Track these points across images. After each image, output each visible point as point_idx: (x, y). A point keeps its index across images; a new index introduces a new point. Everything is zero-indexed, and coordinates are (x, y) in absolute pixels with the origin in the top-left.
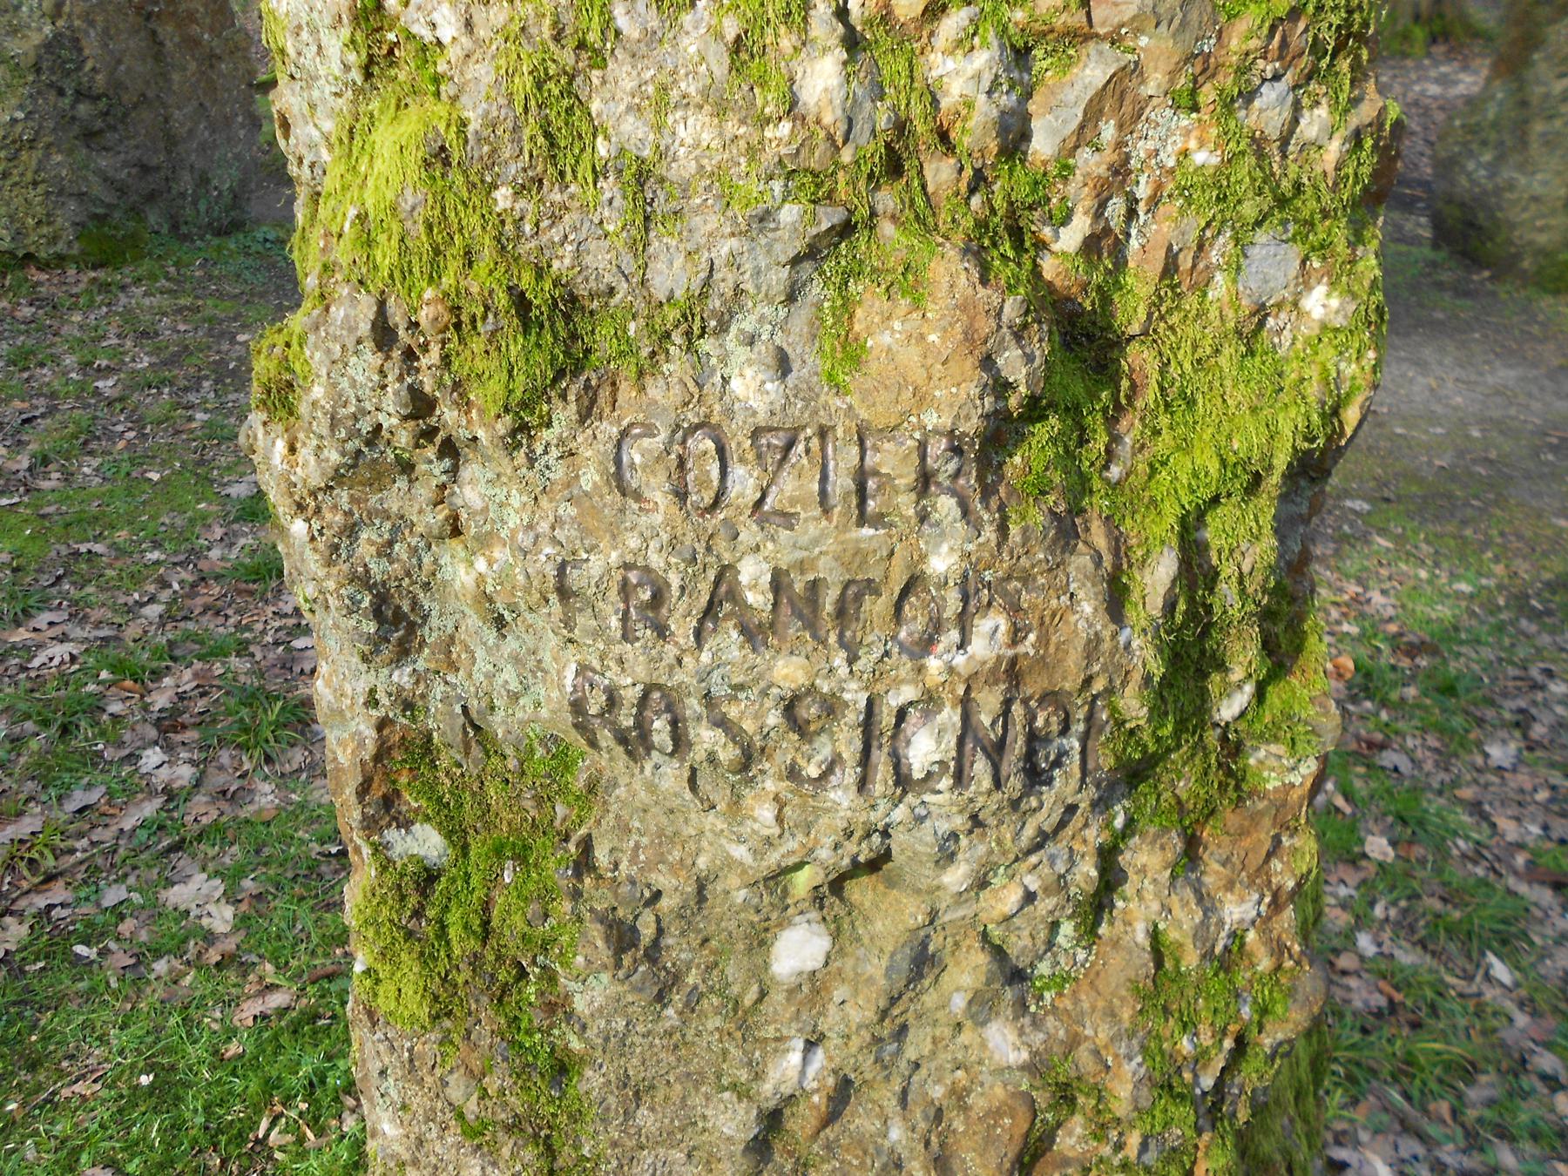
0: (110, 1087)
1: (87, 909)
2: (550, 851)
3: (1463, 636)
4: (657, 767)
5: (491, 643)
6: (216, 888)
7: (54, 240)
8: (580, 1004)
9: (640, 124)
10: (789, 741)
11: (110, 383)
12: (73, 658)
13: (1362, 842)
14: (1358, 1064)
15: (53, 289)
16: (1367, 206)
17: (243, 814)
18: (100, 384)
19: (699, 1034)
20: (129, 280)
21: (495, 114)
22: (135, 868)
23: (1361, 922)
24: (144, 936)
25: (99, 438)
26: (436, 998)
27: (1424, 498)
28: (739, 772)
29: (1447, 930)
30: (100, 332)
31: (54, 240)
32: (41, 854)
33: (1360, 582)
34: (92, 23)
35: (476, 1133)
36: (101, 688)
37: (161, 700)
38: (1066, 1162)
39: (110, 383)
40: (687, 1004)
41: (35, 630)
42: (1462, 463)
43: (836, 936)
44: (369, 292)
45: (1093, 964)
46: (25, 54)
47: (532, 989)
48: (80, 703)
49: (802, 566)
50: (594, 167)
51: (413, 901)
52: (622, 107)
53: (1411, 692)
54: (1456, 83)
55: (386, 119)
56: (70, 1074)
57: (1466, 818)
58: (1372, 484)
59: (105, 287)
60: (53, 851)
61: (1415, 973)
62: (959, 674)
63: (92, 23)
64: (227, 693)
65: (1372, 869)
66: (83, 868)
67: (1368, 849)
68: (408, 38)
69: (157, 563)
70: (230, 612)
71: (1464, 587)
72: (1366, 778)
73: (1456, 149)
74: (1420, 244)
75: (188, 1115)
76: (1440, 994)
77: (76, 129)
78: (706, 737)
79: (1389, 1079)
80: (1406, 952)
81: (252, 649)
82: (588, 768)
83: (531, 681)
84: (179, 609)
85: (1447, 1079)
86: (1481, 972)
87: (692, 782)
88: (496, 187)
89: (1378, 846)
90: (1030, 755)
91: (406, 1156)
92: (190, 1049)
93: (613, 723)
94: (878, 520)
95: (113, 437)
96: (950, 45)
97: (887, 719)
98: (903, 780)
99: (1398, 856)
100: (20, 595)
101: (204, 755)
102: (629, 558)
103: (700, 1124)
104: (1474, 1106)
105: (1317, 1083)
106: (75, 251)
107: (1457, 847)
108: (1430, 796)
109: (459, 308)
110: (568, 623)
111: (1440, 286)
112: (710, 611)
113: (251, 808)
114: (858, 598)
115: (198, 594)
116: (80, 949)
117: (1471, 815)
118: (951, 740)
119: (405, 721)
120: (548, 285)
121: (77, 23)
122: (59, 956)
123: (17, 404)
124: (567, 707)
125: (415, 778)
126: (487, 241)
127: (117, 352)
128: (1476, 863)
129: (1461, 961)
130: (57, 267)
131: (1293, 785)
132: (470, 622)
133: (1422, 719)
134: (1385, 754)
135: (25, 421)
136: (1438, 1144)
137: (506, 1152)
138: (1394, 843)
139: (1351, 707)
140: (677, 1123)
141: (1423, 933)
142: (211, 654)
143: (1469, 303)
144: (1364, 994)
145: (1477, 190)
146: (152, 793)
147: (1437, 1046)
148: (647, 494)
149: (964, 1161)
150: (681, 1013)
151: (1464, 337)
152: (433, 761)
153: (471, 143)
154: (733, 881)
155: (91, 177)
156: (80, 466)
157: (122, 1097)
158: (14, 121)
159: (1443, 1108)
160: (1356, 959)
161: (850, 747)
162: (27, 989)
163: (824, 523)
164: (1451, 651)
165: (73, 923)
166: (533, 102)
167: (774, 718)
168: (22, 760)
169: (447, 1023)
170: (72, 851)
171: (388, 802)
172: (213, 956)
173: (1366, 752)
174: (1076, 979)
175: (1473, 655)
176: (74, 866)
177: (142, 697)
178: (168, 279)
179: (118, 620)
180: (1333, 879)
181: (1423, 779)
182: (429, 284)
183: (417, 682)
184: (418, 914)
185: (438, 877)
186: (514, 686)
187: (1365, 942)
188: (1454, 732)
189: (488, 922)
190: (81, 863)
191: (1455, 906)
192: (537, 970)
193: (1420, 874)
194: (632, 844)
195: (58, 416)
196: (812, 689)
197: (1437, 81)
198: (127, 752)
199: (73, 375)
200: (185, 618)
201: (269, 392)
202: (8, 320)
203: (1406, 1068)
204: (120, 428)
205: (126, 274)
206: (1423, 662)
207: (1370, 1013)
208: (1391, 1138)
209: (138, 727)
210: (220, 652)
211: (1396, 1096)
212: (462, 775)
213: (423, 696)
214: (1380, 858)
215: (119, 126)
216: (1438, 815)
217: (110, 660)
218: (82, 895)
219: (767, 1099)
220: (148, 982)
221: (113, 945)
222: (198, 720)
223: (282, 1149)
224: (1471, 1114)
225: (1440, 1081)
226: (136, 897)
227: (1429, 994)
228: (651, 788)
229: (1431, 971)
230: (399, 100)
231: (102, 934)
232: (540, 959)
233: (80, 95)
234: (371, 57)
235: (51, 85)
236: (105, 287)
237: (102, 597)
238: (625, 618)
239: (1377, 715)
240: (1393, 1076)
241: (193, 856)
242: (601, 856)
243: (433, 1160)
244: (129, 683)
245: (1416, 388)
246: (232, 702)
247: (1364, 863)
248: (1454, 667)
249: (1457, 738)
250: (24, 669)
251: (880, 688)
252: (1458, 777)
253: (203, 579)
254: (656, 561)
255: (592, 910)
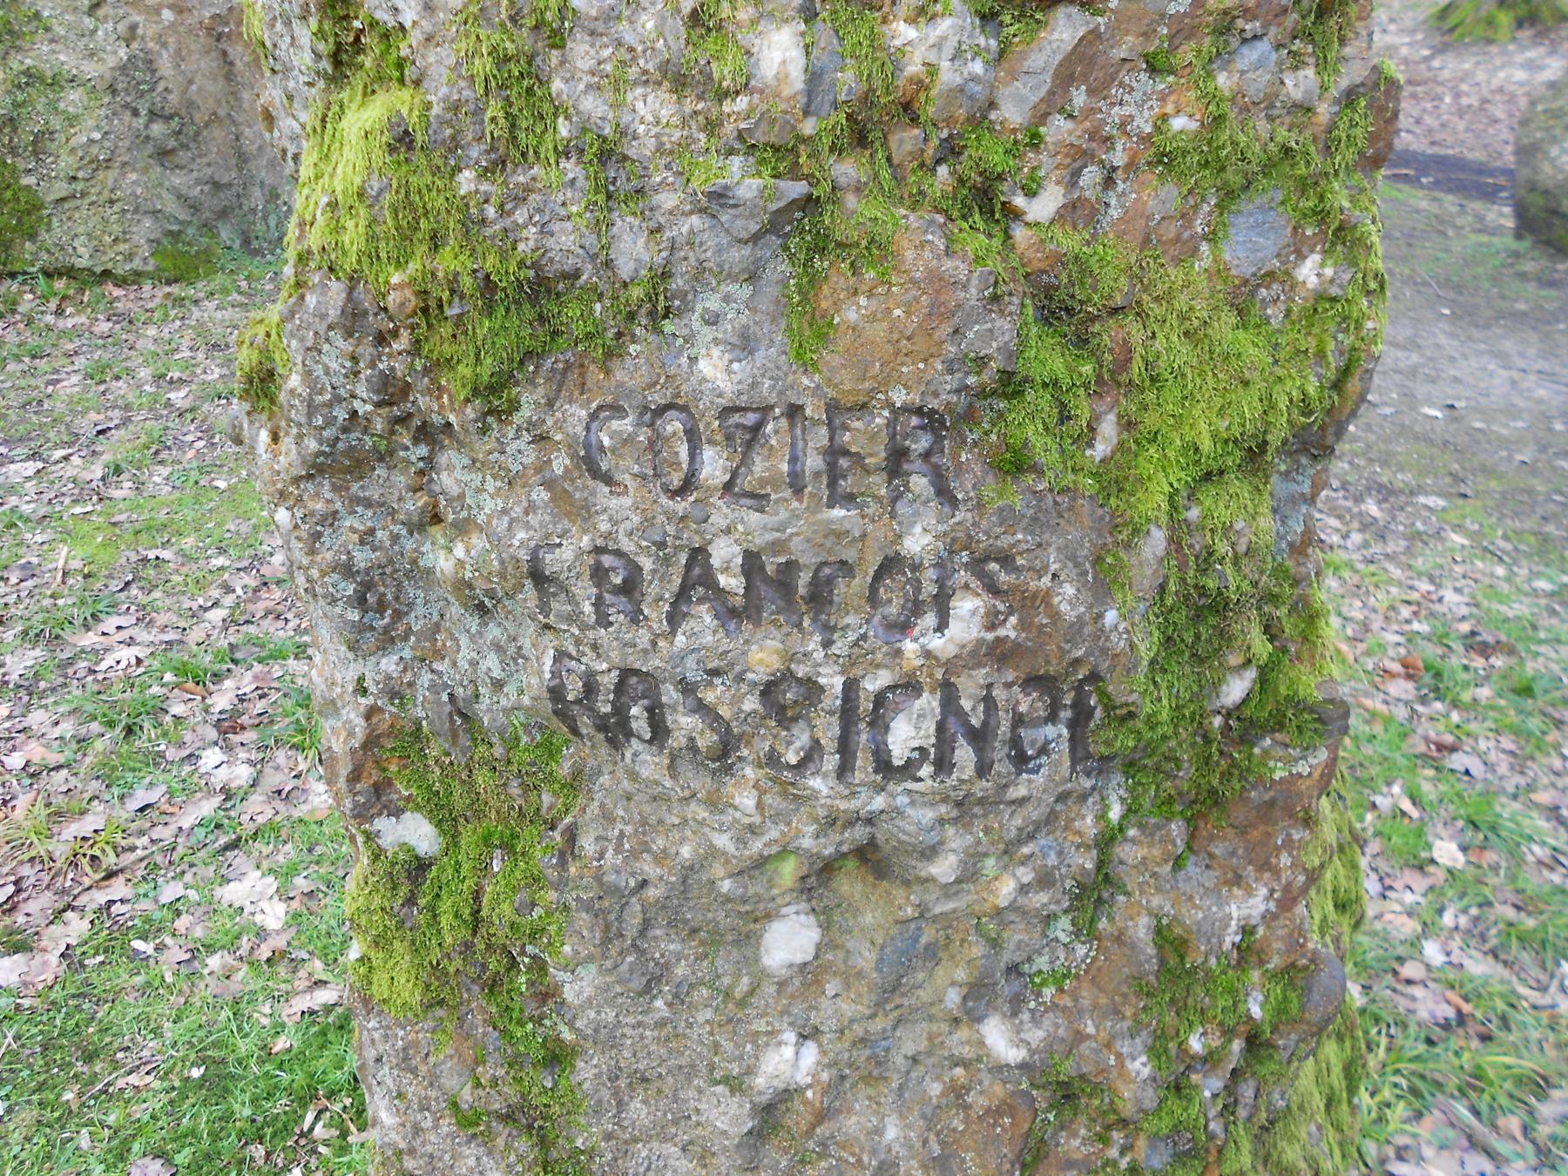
0: (161, 1079)
1: (145, 904)
2: (536, 839)
3: (1542, 635)
4: (635, 755)
5: (473, 630)
6: (270, 885)
7: (130, 257)
8: (568, 993)
9: (599, 102)
10: (767, 728)
11: (182, 394)
12: (139, 661)
13: (1429, 847)
14: (1423, 1077)
15: (130, 305)
16: (1363, 170)
17: (296, 814)
18: (172, 395)
19: (690, 1026)
20: (201, 295)
21: (456, 97)
22: (192, 865)
23: (1427, 929)
24: (199, 932)
25: (169, 448)
26: (428, 986)
27: (1503, 493)
28: (718, 759)
29: (1520, 939)
30: (174, 345)
31: (130, 257)
32: (103, 851)
33: (1432, 580)
34: (164, 45)
35: (468, 1120)
36: (164, 690)
37: (222, 701)
38: (1070, 1164)
39: (182, 394)
40: (676, 996)
41: (104, 634)
42: (1544, 456)
43: (826, 927)
44: (338, 279)
45: (1094, 959)
46: (101, 77)
47: (522, 979)
48: (144, 704)
49: (777, 547)
50: (556, 148)
51: (403, 891)
52: (582, 87)
53: (1484, 693)
54: (1541, 68)
55: (354, 106)
56: (124, 1065)
57: (1542, 824)
58: (1448, 480)
59: (179, 301)
60: (115, 848)
61: (1486, 984)
62: (936, 658)
63: (164, 45)
64: (285, 695)
65: (1441, 875)
66: (143, 865)
67: (1436, 855)
68: (371, 25)
69: (221, 568)
70: (289, 616)
71: (1542, 584)
72: (1435, 781)
73: (1538, 135)
74: (1502, 235)
75: (236, 1107)
76: (1513, 1006)
77: (150, 149)
78: (684, 723)
79: (1456, 1093)
80: (1477, 961)
81: (310, 651)
82: (572, 756)
83: (513, 668)
84: (242, 613)
85: (1517, 1093)
86: (1555, 982)
87: (671, 767)
88: (460, 170)
89: (1447, 852)
90: (1015, 742)
91: (402, 1145)
92: (240, 1043)
93: (592, 709)
94: (849, 499)
95: (182, 446)
96: (912, 14)
97: (866, 705)
98: (883, 764)
99: (1469, 862)
100: (90, 601)
101: (261, 755)
102: (600, 542)
103: (694, 1118)
104: (1546, 1122)
105: (1352, 1090)
106: (150, 268)
107: (1533, 853)
108: (1504, 800)
109: (425, 292)
110: (544, 608)
111: (1523, 276)
112: (683, 595)
113: (305, 808)
114: (830, 581)
115: (260, 599)
116: (138, 944)
117: (1548, 820)
118: (930, 727)
119: (394, 710)
120: (512, 267)
121: (151, 45)
122: (118, 951)
123: (93, 416)
124: (546, 695)
125: (405, 767)
126: (452, 225)
127: (189, 365)
128: (1552, 869)
129: (1535, 972)
130: (134, 283)
131: (1300, 775)
132: (453, 609)
133: (1496, 721)
134: (1455, 756)
135: (100, 432)
136: (1507, 1161)
137: (500, 1142)
138: (1464, 849)
139: (1420, 708)
140: (669, 1116)
141: (1493, 942)
142: (271, 657)
143: (1553, 293)
144: (1430, 1004)
145: (1560, 177)
146: (210, 792)
147: (1507, 1060)
148: (618, 477)
149: (963, 1160)
150: (670, 1005)
151: (1548, 328)
152: (422, 749)
153: (434, 126)
154: (718, 870)
155: (165, 194)
156: (151, 475)
157: (173, 1088)
158: (92, 141)
159: (1513, 1123)
160: (1423, 968)
161: (828, 731)
162: (87, 983)
163: (795, 504)
164: (1528, 651)
165: (132, 919)
166: (493, 84)
167: (751, 704)
168: (88, 760)
169: (440, 1012)
170: (133, 849)
171: (379, 789)
172: (264, 952)
173: (1435, 754)
174: (1077, 976)
175: (1553, 655)
176: (134, 863)
177: (204, 698)
178: (240, 293)
179: (182, 624)
180: (1398, 885)
181: (1496, 782)
182: (396, 269)
183: (405, 670)
184: (411, 901)
185: (431, 865)
186: (497, 673)
187: (1432, 951)
188: (1529, 734)
189: (478, 911)
190: (141, 860)
191: (1529, 914)
192: (527, 960)
193: (1492, 880)
194: (616, 832)
195: (131, 427)
196: (788, 675)
197: (1522, 66)
198: (187, 752)
199: (147, 387)
200: (247, 622)
201: (251, 382)
202: (87, 335)
203: (1473, 1083)
204: (190, 438)
205: (199, 289)
206: (1498, 661)
207: (1437, 1024)
208: (1458, 1153)
209: (198, 728)
210: (278, 655)
211: (1462, 1110)
212: (451, 763)
213: (411, 684)
214: (1449, 864)
215: (192, 145)
216: (1512, 819)
217: (174, 663)
218: (141, 891)
219: (760, 1093)
220: (202, 977)
221: (169, 941)
222: (257, 721)
223: (326, 1143)
224: (1543, 1131)
225: (1511, 1096)
226: (193, 895)
227: (1500, 1005)
228: (633, 776)
229: (1502, 981)
230: (366, 87)
231: (159, 930)
232: (529, 949)
233: (153, 115)
234: (338, 45)
235: (126, 106)
236: (179, 301)
237: (168, 602)
238: (598, 603)
239: (1447, 716)
240: (1460, 1090)
241: (249, 853)
242: (587, 844)
243: (429, 1149)
244: (190, 685)
245: (1497, 381)
246: (289, 704)
247: (1431, 869)
248: (1531, 667)
249: (1533, 741)
250: (92, 672)
251: (857, 672)
252: (1534, 780)
253: (265, 584)
254: (627, 545)
255: (578, 899)
